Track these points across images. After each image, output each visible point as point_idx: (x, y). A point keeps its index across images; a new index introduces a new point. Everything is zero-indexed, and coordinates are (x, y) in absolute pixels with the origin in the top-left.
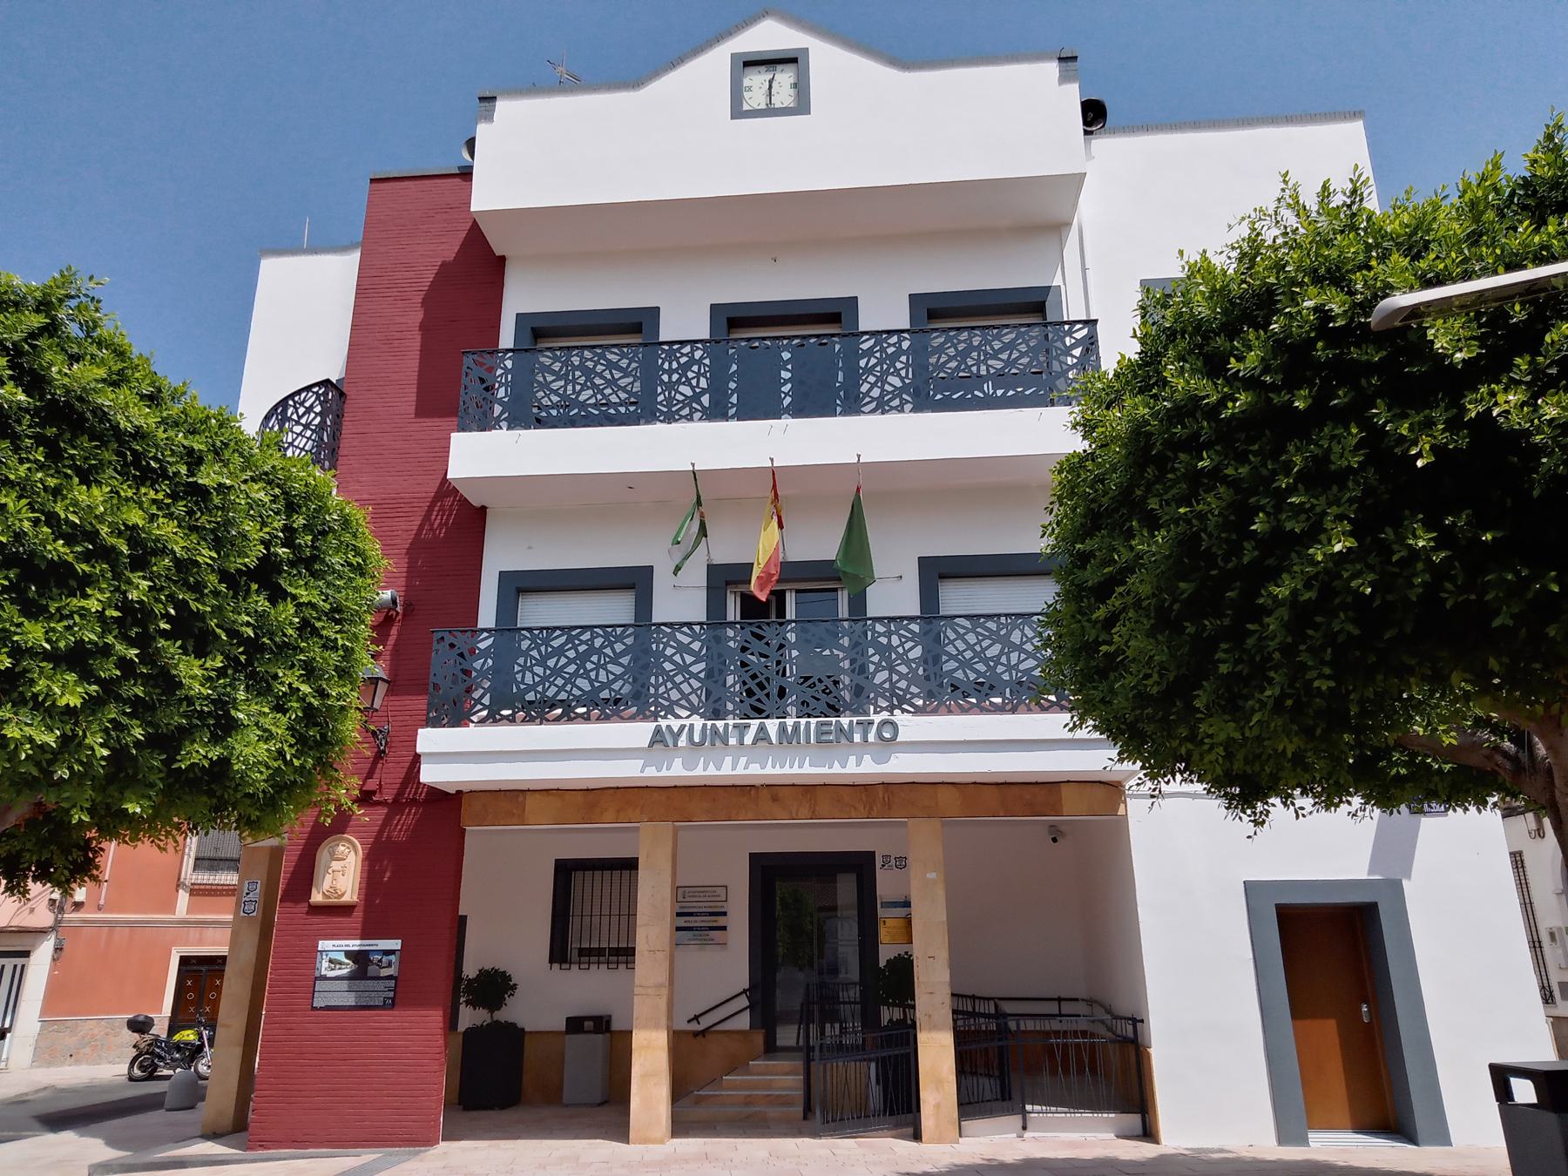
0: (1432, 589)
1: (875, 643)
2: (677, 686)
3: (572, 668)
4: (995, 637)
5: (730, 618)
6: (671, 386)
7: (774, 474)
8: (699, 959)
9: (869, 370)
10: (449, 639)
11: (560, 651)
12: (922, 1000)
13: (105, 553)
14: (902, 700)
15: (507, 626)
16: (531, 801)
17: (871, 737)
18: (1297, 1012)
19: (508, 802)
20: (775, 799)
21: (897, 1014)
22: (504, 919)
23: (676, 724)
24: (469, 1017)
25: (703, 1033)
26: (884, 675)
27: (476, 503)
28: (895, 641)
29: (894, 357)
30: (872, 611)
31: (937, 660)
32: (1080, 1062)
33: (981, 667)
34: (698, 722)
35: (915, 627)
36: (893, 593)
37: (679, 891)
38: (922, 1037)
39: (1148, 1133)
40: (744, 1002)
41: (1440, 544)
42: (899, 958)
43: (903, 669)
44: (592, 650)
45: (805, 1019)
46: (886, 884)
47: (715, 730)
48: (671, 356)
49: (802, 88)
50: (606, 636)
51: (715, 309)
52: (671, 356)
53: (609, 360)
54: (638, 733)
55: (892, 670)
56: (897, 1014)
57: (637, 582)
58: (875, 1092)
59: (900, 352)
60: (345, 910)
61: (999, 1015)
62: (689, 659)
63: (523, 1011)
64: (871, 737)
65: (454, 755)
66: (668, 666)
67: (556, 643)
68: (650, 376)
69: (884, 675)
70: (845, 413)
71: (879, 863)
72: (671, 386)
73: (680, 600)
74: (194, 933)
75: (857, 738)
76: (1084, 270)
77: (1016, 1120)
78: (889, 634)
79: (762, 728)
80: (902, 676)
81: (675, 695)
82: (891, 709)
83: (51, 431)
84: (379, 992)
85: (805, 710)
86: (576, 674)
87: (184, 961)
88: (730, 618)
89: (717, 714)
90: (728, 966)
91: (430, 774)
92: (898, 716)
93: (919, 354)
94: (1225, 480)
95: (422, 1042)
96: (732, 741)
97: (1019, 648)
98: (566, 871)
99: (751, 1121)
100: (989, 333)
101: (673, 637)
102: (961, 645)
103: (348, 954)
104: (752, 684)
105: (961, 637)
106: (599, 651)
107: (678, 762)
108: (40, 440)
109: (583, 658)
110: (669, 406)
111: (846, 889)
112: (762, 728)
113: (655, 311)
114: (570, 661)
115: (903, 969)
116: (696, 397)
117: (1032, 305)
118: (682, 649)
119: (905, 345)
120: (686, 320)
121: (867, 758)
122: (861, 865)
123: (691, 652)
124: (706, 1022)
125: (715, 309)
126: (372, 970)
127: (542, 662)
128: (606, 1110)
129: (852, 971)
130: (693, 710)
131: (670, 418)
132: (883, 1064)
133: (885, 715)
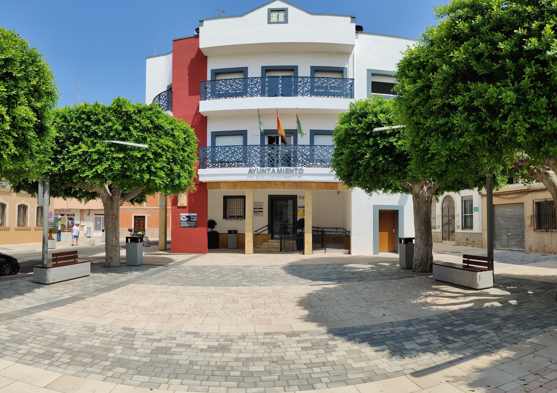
0: (383, 166)
1: (299, 151)
2: (254, 160)
3: (230, 155)
4: (326, 151)
5: (266, 144)
6: (252, 88)
7: (277, 110)
8: (258, 218)
9: (300, 86)
10: (203, 149)
11: (227, 152)
12: (306, 228)
13: (164, 150)
14: (305, 164)
15: (213, 145)
16: (222, 184)
17: (297, 172)
18: (380, 230)
19: (217, 185)
20: (276, 185)
21: (301, 231)
22: (215, 210)
23: (254, 168)
24: (210, 230)
25: (258, 234)
26: (301, 158)
27: (205, 116)
28: (304, 150)
29: (306, 83)
30: (299, 143)
31: (312, 155)
32: (338, 240)
33: (322, 157)
34: (259, 168)
35: (308, 148)
36: (304, 140)
37: (255, 203)
38: (305, 235)
39: (349, 253)
40: (267, 228)
41: (384, 160)
42: (302, 219)
43: (305, 157)
44: (235, 151)
45: (280, 233)
46: (299, 203)
47: (263, 170)
48: (252, 81)
49: (286, 17)
50: (238, 148)
51: (263, 67)
52: (252, 81)
53: (237, 82)
54: (246, 170)
55: (303, 157)
56: (301, 231)
57: (243, 134)
58: (295, 246)
59: (307, 82)
60: (185, 207)
61: (323, 231)
62: (257, 153)
63: (217, 229)
64: (297, 172)
65: (206, 175)
66: (252, 155)
67: (226, 150)
68: (246, 86)
69: (301, 158)
70: (295, 96)
71: (298, 197)
72: (252, 88)
73: (254, 139)
74: (136, 211)
75: (294, 172)
76: (353, 64)
77: (324, 251)
78: (302, 149)
79: (273, 170)
80: (305, 159)
81: (254, 162)
82: (302, 166)
83: (156, 131)
84: (193, 224)
85: (283, 165)
86: (231, 157)
87: (135, 217)
88: (266, 144)
89: (263, 166)
90: (264, 220)
91: (201, 179)
92: (304, 168)
93: (312, 83)
94: (357, 143)
95: (203, 232)
96: (267, 172)
97: (330, 153)
98: (226, 198)
99: (269, 251)
100: (330, 77)
101: (253, 148)
102: (318, 152)
103: (186, 216)
104: (271, 159)
105: (318, 150)
106: (236, 151)
107: (255, 177)
108: (155, 133)
109: (233, 153)
110: (252, 93)
111: (290, 202)
112: (273, 170)
113: (247, 68)
114: (230, 154)
115: (302, 221)
116: (258, 91)
117: (341, 71)
118: (255, 151)
119: (309, 80)
120: (255, 72)
121: (296, 177)
122: (294, 198)
123: (258, 152)
124: (258, 232)
125: (263, 67)
126: (191, 219)
127: (224, 154)
128: (240, 247)
129: (291, 222)
130: (258, 165)
131: (252, 96)
132: (297, 240)
133: (301, 167)
